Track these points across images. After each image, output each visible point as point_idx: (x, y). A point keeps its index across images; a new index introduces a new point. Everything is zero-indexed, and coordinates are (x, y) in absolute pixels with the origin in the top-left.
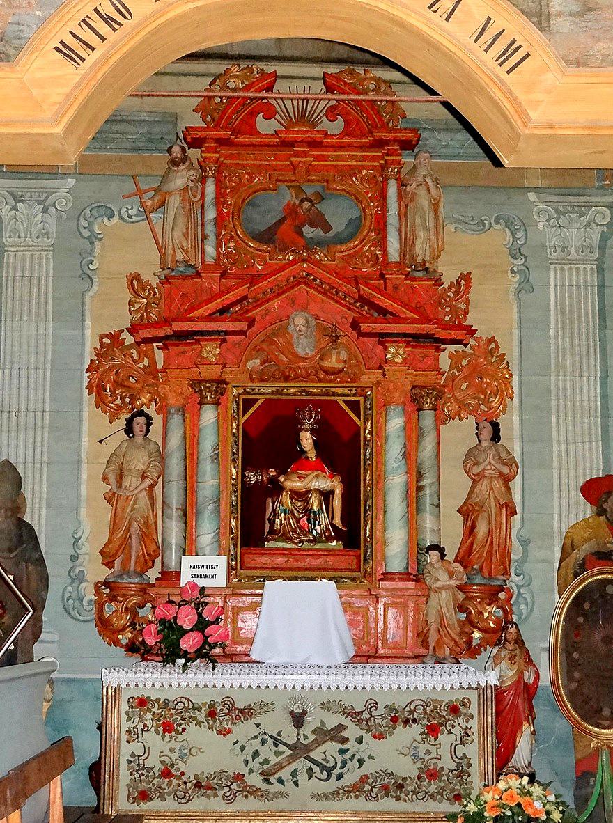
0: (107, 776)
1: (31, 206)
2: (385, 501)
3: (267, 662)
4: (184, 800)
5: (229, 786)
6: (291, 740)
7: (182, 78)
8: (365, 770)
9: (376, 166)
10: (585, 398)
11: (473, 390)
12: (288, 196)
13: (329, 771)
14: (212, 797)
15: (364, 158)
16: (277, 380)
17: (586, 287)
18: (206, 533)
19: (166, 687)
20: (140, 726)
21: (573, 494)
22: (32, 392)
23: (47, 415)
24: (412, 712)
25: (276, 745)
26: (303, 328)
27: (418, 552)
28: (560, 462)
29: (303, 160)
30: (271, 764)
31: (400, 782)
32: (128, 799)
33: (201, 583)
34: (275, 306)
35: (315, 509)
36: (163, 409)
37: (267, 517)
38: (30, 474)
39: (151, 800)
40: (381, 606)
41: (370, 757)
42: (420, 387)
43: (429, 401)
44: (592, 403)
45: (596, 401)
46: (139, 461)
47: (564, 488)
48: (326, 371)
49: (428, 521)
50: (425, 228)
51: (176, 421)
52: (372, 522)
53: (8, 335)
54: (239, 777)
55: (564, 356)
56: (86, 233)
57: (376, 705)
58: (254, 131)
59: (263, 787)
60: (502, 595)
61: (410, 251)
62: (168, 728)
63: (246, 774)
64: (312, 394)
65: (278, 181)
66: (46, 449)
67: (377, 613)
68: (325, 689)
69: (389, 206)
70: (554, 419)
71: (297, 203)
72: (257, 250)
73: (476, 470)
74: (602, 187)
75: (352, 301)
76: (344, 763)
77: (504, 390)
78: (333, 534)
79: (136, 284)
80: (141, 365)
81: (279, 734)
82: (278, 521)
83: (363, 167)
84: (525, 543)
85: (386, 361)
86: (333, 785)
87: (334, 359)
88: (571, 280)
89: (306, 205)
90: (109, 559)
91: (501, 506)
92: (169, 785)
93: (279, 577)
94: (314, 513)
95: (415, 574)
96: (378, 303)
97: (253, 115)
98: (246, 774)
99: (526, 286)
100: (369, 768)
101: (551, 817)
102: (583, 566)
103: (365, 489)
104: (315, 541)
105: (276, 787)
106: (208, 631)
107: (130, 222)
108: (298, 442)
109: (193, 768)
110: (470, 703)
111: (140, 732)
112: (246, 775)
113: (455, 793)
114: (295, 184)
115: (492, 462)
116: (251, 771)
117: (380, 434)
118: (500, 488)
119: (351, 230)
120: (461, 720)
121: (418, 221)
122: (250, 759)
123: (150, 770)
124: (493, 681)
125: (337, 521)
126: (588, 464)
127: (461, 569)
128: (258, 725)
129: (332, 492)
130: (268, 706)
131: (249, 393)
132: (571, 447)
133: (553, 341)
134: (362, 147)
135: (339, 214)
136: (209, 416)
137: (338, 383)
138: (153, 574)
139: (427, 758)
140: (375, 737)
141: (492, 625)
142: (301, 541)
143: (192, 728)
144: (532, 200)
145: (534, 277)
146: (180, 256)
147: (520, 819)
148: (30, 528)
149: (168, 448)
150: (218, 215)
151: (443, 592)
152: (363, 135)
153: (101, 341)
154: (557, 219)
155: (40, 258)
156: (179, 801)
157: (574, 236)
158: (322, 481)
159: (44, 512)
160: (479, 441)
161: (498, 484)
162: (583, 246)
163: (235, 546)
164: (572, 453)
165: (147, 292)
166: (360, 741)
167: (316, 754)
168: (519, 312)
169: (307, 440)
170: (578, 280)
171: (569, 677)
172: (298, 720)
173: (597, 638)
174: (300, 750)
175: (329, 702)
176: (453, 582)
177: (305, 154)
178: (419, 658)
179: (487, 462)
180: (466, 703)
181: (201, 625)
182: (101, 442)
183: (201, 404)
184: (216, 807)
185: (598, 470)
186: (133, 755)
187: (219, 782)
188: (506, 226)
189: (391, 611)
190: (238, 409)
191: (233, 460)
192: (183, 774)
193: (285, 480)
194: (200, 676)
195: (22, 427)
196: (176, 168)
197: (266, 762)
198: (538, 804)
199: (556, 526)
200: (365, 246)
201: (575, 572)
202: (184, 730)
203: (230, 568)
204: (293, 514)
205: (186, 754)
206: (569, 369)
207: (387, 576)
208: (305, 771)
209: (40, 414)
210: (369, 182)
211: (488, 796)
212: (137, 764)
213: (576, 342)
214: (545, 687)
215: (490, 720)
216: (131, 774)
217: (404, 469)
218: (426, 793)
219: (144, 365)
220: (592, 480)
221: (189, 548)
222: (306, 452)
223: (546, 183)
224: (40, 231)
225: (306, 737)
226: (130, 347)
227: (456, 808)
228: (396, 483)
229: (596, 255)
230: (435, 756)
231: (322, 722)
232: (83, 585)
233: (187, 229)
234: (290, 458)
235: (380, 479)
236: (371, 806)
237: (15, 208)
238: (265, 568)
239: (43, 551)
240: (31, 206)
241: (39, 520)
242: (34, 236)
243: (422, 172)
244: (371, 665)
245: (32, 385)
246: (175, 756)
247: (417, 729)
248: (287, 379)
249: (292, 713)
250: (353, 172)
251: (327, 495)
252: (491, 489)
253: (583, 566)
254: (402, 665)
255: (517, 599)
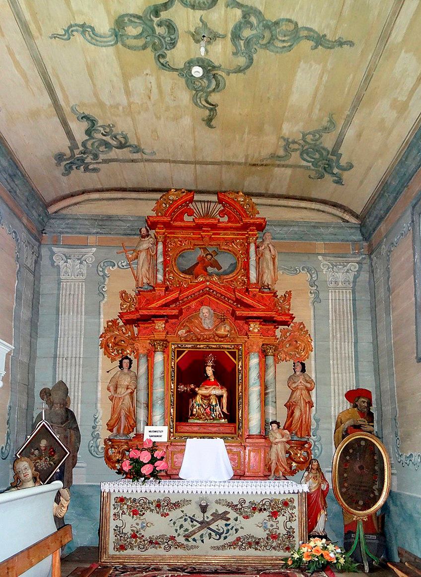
0: (103, 538)
1: (74, 261)
2: (249, 399)
3: (188, 479)
4: (143, 550)
5: (167, 542)
6: (200, 519)
7: (148, 201)
8: (239, 534)
9: (244, 238)
10: (347, 352)
11: (292, 348)
12: (200, 253)
13: (220, 535)
14: (158, 548)
15: (239, 234)
16: (194, 341)
17: (347, 300)
18: (158, 415)
19: (135, 492)
20: (121, 512)
21: (341, 398)
22: (74, 348)
23: (81, 359)
24: (263, 505)
25: (192, 522)
26: (207, 315)
27: (265, 425)
28: (334, 382)
29: (207, 234)
30: (189, 531)
31: (257, 540)
32: (114, 549)
33: (154, 439)
34: (193, 304)
35: (214, 404)
36: (137, 357)
37: (190, 408)
38: (72, 387)
39: (126, 550)
40: (247, 451)
41: (242, 528)
42: (267, 345)
43: (271, 351)
44: (350, 355)
45: (352, 354)
46: (126, 381)
47: (337, 395)
48: (217, 335)
49: (271, 410)
50: (269, 269)
51: (143, 361)
52: (242, 410)
53: (63, 321)
54: (173, 538)
55: (336, 333)
56: (101, 274)
57: (244, 501)
58: (182, 220)
59: (185, 543)
60: (306, 446)
61: (261, 279)
62: (135, 513)
63: (176, 536)
64: (212, 348)
65: (195, 245)
66: (81, 376)
67: (245, 455)
68: (218, 493)
69: (250, 256)
70: (331, 362)
71: (205, 256)
72: (184, 278)
73: (294, 385)
74: (354, 254)
75: (232, 302)
76: (228, 531)
77: (307, 348)
78: (222, 416)
79: (124, 296)
80: (127, 335)
81: (194, 516)
82: (195, 410)
83: (238, 239)
84: (317, 421)
85: (249, 331)
86: (222, 542)
87: (223, 330)
88: (339, 297)
89: (209, 257)
90: (110, 428)
91: (306, 403)
92: (136, 542)
93: (195, 437)
94: (213, 406)
95: (264, 435)
96: (246, 302)
97: (182, 213)
98: (176, 536)
99: (317, 300)
100: (241, 533)
101: (339, 561)
102: (346, 433)
103: (238, 394)
104: (213, 419)
105: (192, 543)
106: (156, 464)
107: (122, 268)
108: (205, 371)
109: (148, 533)
110: (294, 500)
111: (120, 514)
112: (176, 537)
113: (287, 546)
114: (204, 246)
115: (302, 382)
116: (179, 535)
117: (246, 366)
118: (306, 394)
119: (231, 269)
120: (289, 509)
121: (265, 265)
122: (178, 528)
123: (125, 534)
124: (306, 489)
125: (225, 410)
126: (348, 383)
127: (288, 433)
128: (182, 511)
129: (222, 396)
130: (189, 502)
131: (180, 348)
132: (340, 375)
133: (330, 325)
134: (237, 229)
135: (226, 261)
136: (159, 357)
137: (225, 342)
138: (132, 435)
139: (271, 528)
140: (244, 518)
141: (302, 460)
142: (207, 419)
143: (148, 513)
144: (320, 259)
145: (321, 295)
146: (145, 281)
147: (323, 562)
148: (72, 414)
149: (139, 373)
150: (164, 261)
151: (279, 444)
152: (237, 222)
153: (107, 324)
154: (333, 268)
155: (79, 285)
156: (141, 550)
157: (340, 276)
158: (218, 391)
159: (79, 405)
160: (295, 372)
161: (305, 392)
162: (345, 281)
163: (173, 421)
164: (340, 377)
165: (129, 300)
166: (236, 520)
167: (213, 526)
168: (314, 312)
169: (209, 371)
170: (343, 297)
171: (341, 486)
172: (204, 509)
173: (356, 467)
174: (204, 524)
175: (220, 500)
176: (284, 440)
177: (208, 231)
178: (266, 477)
179: (299, 382)
180: (292, 501)
181: (153, 461)
182: (108, 372)
183: (155, 352)
184: (160, 553)
185: (354, 386)
186: (117, 526)
187: (162, 540)
188: (308, 272)
189: (252, 454)
190: (175, 355)
191: (172, 380)
192: (143, 536)
193: (198, 390)
194: (152, 486)
195: (69, 365)
196: (144, 239)
197: (187, 530)
198: (332, 555)
199: (333, 413)
200: (238, 276)
201: (343, 435)
202: (144, 514)
203: (170, 432)
204: (202, 406)
205: (144, 526)
206: (339, 338)
207: (250, 436)
208: (207, 535)
209: (78, 359)
210: (241, 245)
211: (304, 550)
212: (119, 531)
213: (342, 326)
214: (331, 489)
215: (304, 509)
216: (116, 536)
217: (258, 384)
218: (271, 546)
219: (129, 335)
220: (350, 391)
221: (149, 422)
222: (209, 377)
223: (327, 251)
224: (78, 273)
225: (208, 518)
226: (122, 326)
227: (287, 554)
228: (254, 391)
229: (351, 285)
230: (276, 527)
231: (216, 510)
232: (99, 440)
233: (149, 268)
234: (202, 380)
235: (246, 389)
236: (242, 553)
237: (66, 262)
238: (188, 432)
239: (79, 424)
240: (74, 261)
241: (77, 409)
242: (76, 274)
243: (267, 242)
244: (242, 481)
245: (74, 345)
246: (139, 527)
247: (266, 513)
248: (199, 340)
249: (200, 505)
250: (233, 241)
251: (219, 398)
252: (301, 394)
253: (346, 433)
254: (258, 481)
255: (314, 447)
